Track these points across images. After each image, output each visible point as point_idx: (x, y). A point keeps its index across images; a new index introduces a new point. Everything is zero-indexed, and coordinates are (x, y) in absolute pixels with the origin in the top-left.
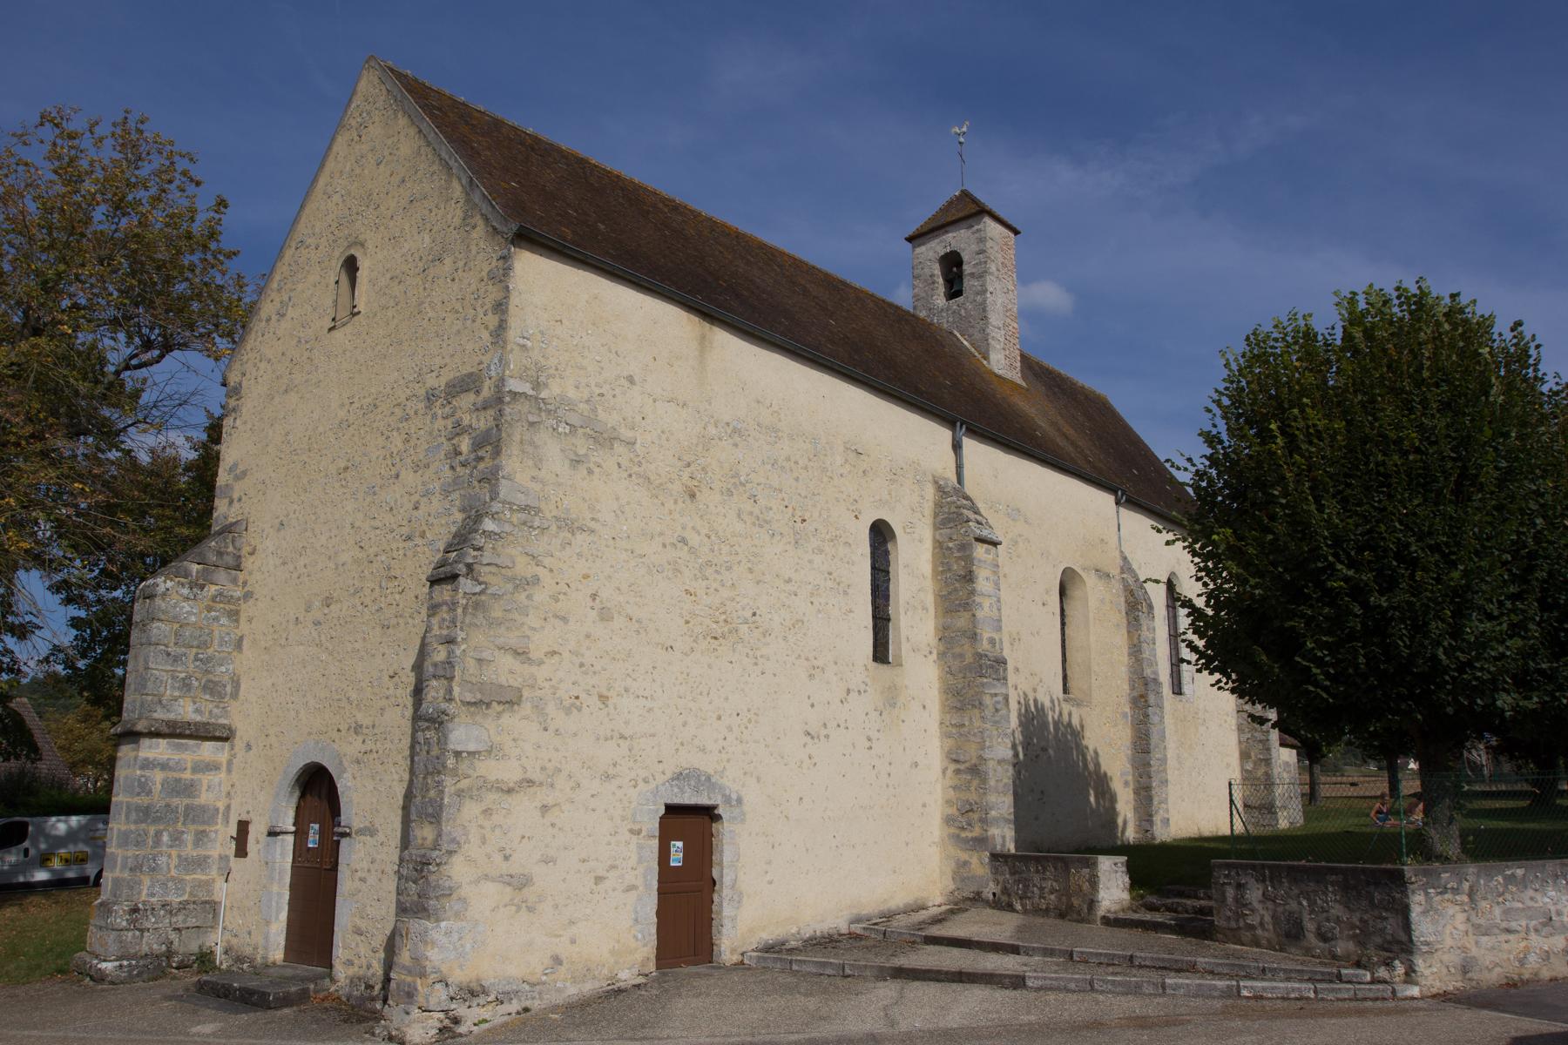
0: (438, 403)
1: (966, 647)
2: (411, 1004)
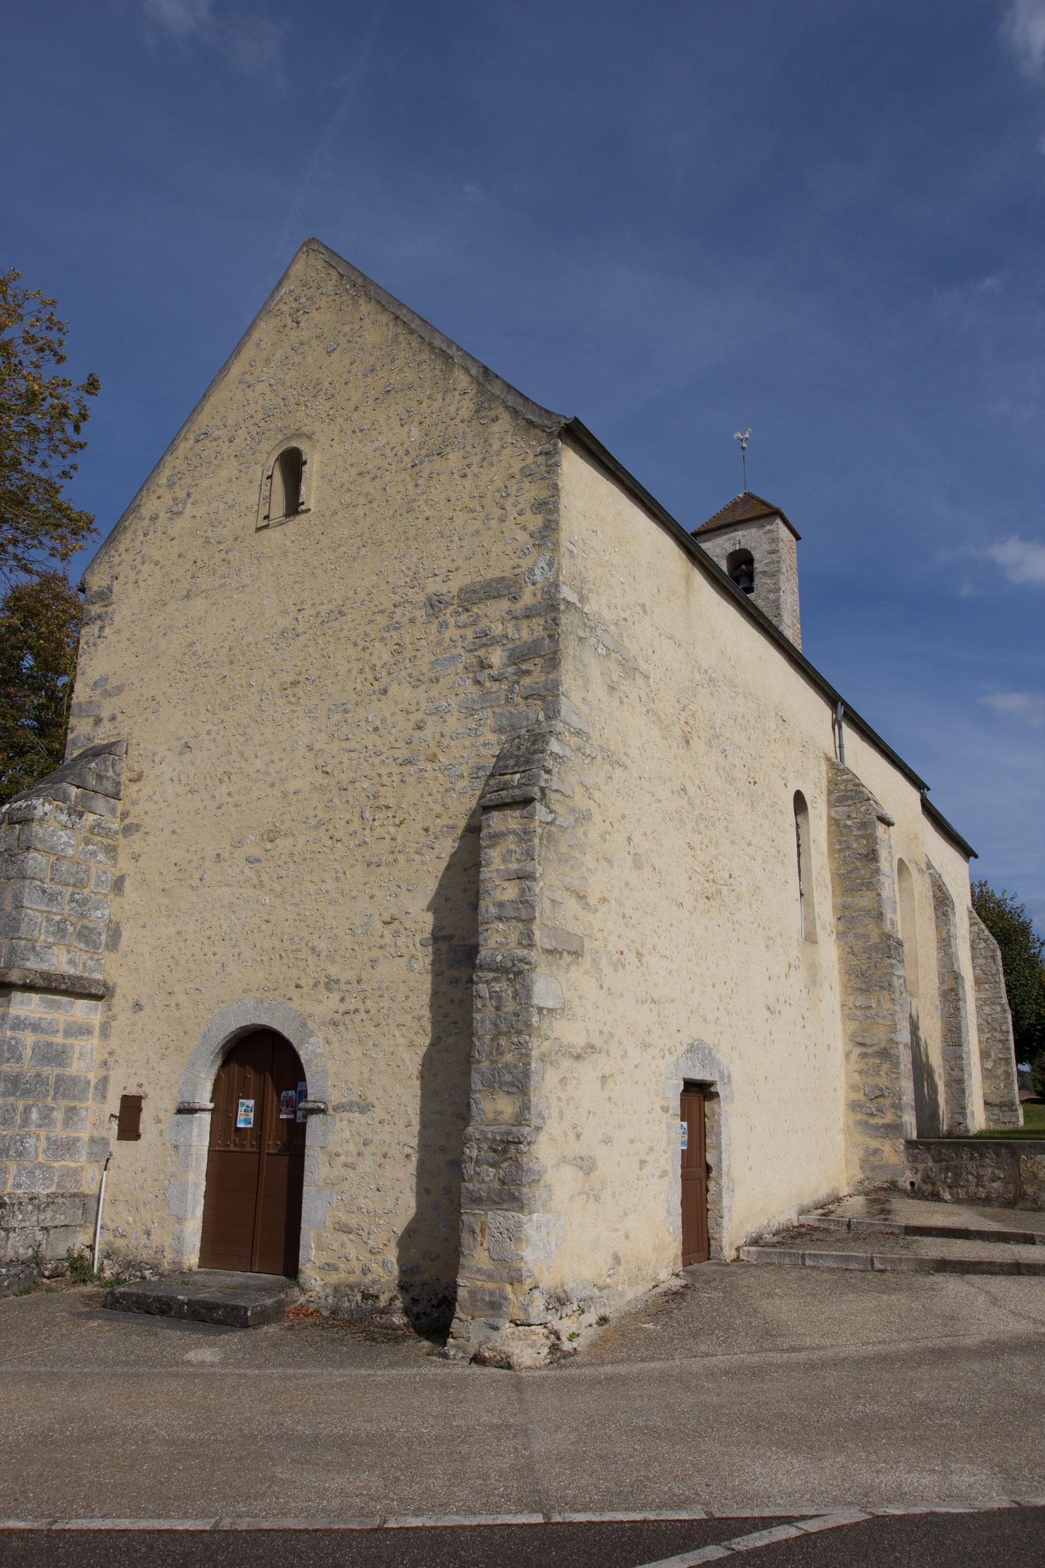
0: (449, 610)
1: (871, 927)
2: (500, 1316)
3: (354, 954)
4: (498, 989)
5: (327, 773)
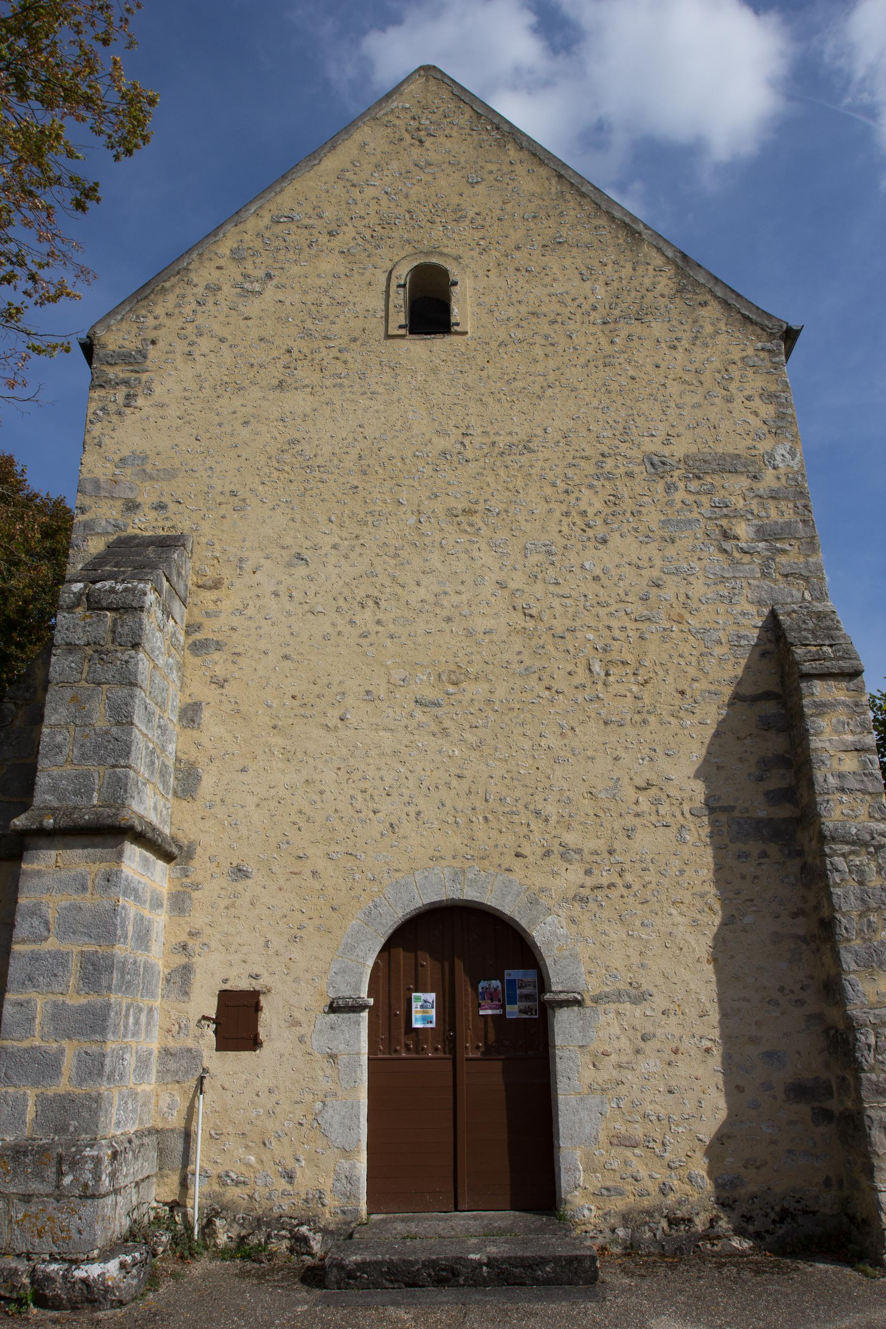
3: (598, 820)
4: (858, 863)
5: (531, 616)
